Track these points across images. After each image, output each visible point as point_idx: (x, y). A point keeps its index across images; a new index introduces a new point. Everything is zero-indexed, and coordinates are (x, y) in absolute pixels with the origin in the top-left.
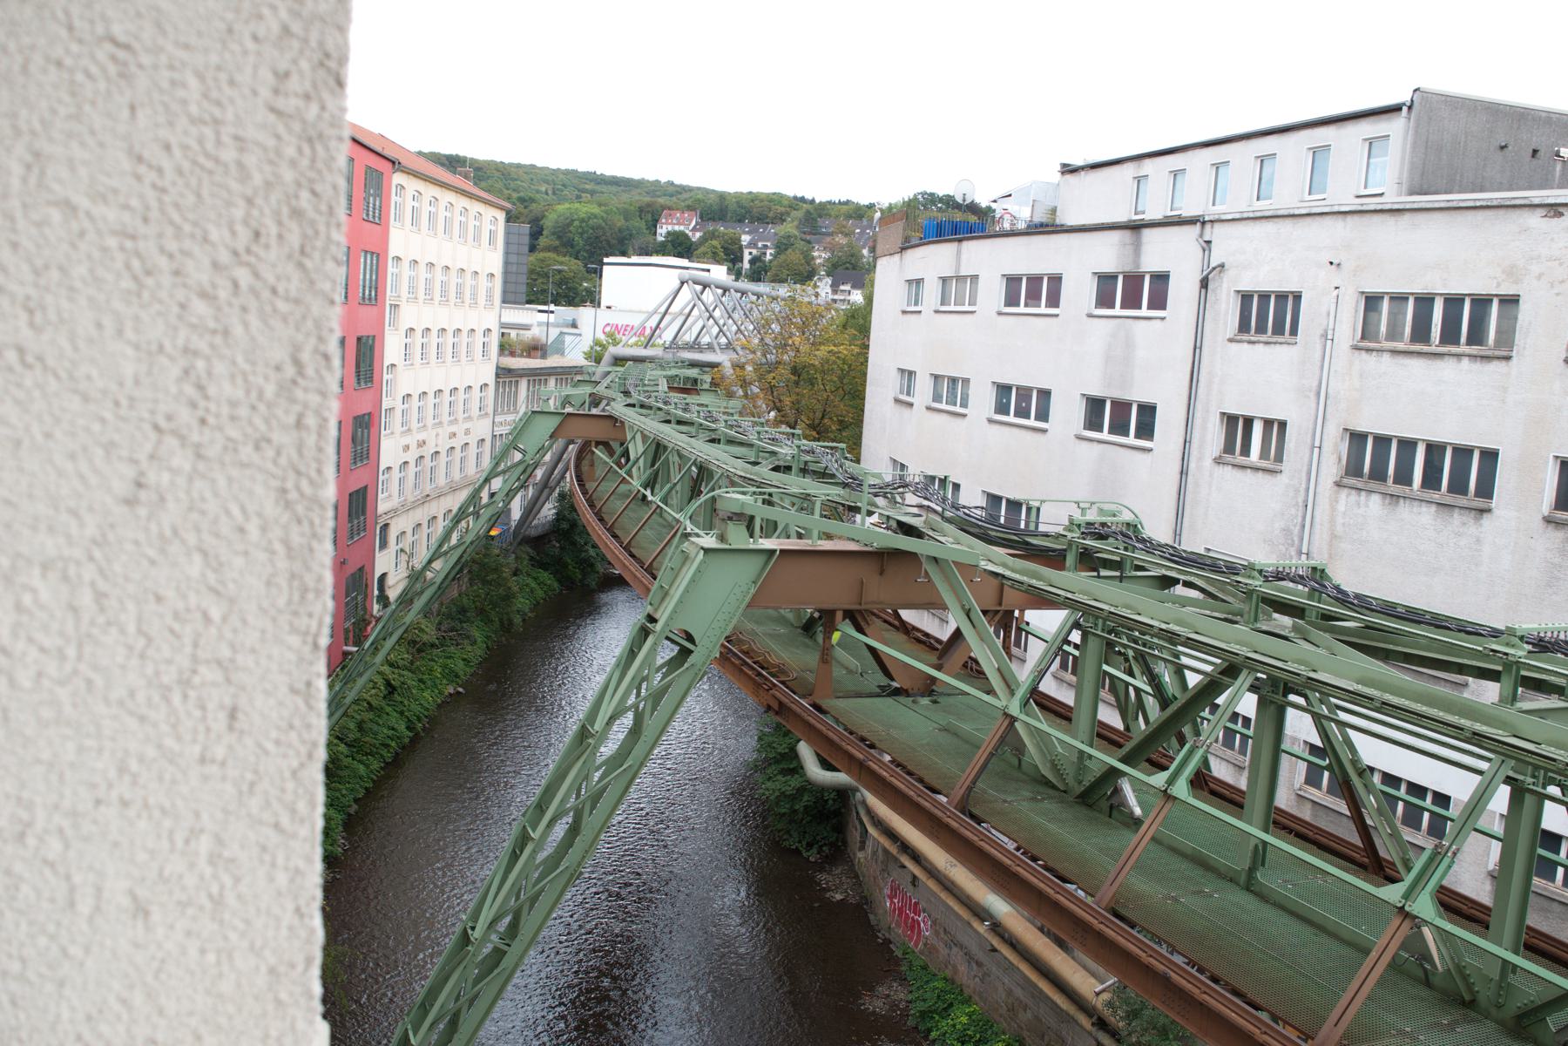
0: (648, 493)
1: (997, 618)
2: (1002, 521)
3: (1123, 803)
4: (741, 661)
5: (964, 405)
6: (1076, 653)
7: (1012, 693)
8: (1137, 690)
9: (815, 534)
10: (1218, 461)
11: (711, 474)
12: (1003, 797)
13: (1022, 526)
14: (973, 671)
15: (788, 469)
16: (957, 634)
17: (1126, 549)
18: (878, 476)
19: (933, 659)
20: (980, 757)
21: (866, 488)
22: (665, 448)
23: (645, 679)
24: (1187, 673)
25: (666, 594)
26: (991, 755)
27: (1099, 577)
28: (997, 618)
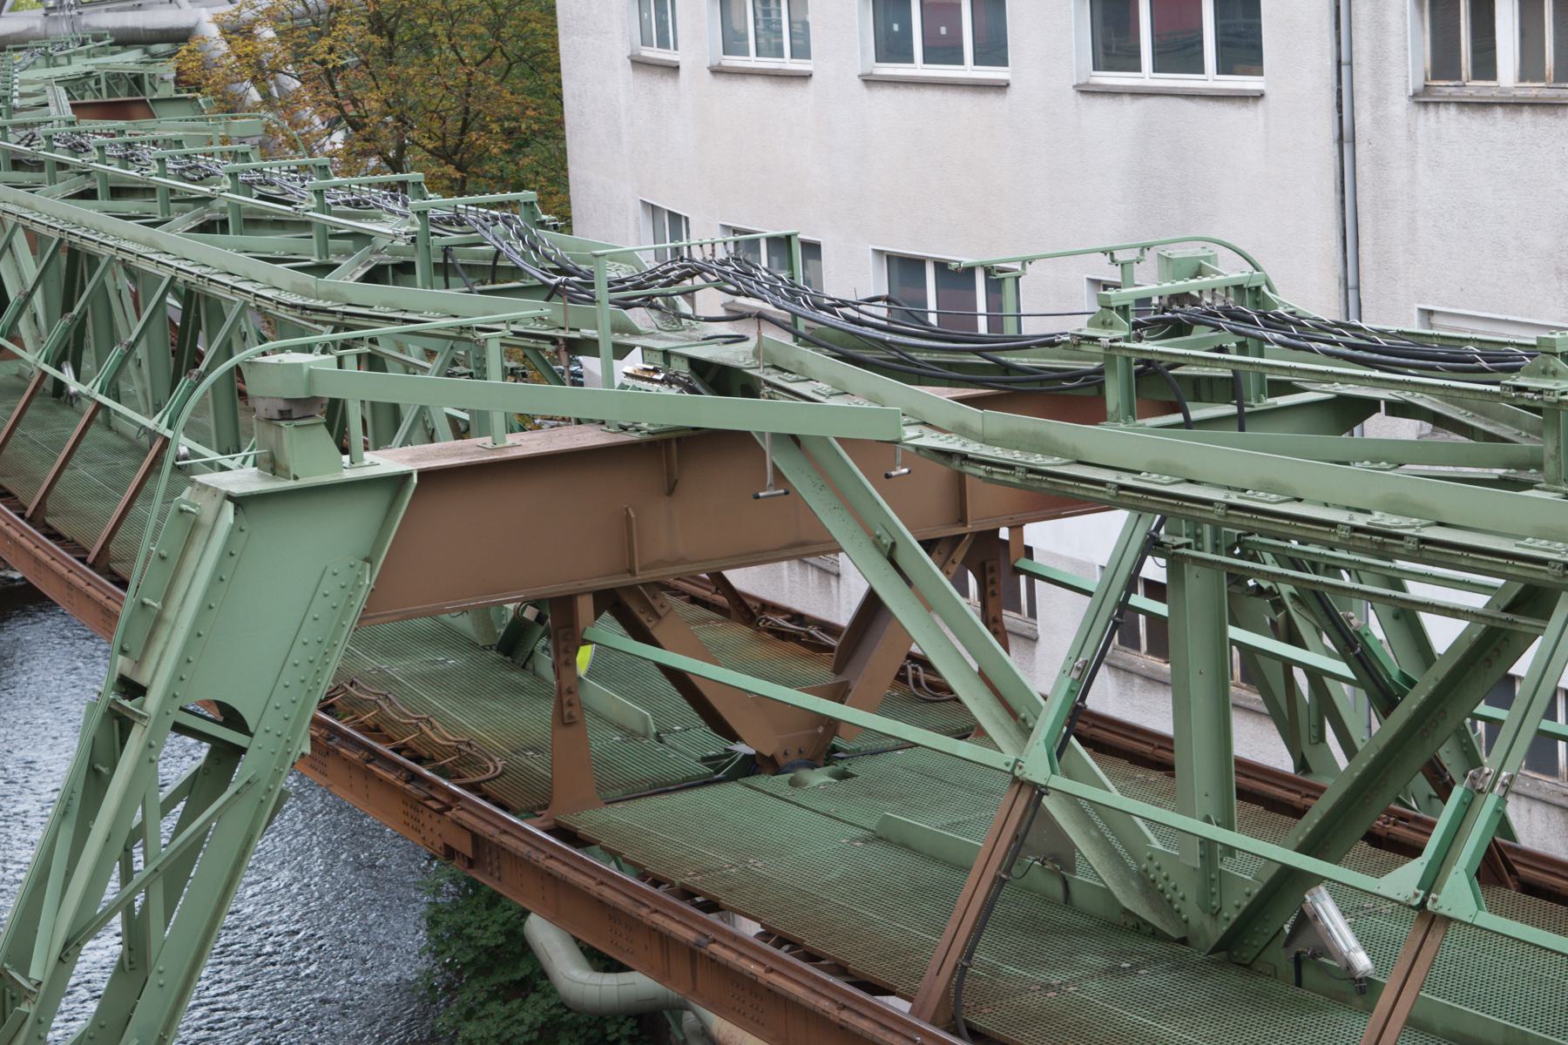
0: (67, 376)
1: (960, 554)
2: (933, 319)
3: (1324, 948)
4: (360, 747)
5: (801, 50)
6: (1161, 609)
7: (1025, 730)
8: (1314, 674)
9: (498, 421)
10: (1423, 99)
11: (216, 309)
12: (1041, 977)
13: (983, 328)
14: (921, 688)
15: (404, 270)
16: (872, 606)
17: (1242, 348)
18: (627, 257)
19: (822, 672)
20: (973, 890)
21: (601, 291)
22: (93, 260)
23: (138, 834)
24: (1426, 619)
25: (159, 619)
26: (999, 883)
27: (1188, 424)
28: (960, 554)
